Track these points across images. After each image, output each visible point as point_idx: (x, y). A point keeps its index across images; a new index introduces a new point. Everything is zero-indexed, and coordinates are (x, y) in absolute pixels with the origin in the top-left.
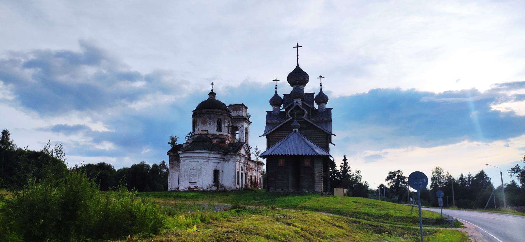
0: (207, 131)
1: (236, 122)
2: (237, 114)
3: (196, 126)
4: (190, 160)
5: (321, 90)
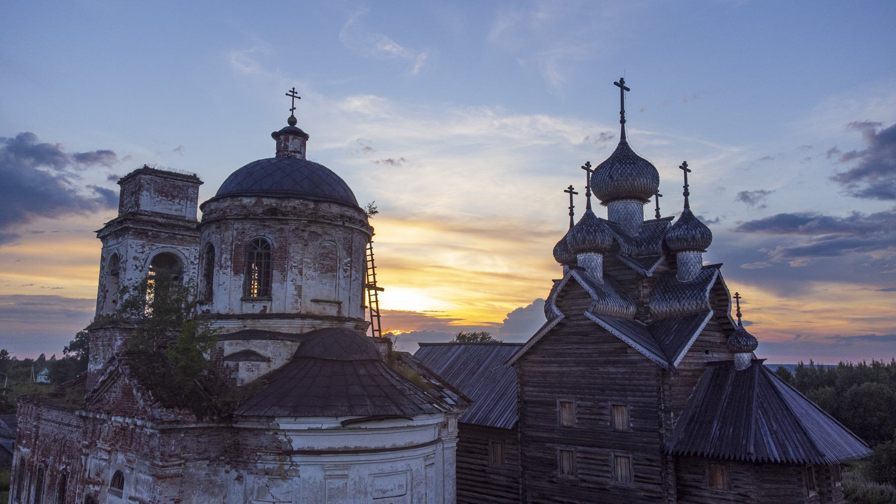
0: (339, 303)
1: (176, 239)
2: (176, 210)
3: (276, 274)
4: (374, 468)
5: (687, 205)
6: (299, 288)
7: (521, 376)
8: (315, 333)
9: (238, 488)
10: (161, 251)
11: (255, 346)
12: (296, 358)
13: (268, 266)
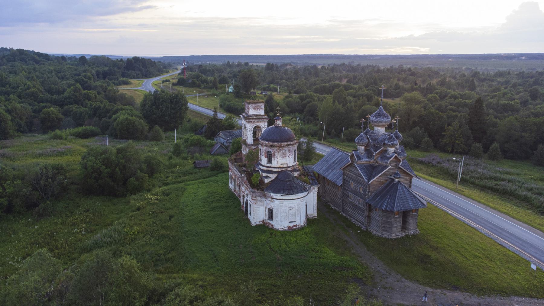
3: (273, 159)
6: (278, 162)
7: (344, 173)
8: (281, 171)
9: (265, 202)
10: (255, 125)
11: (269, 175)
12: (277, 177)
13: (271, 157)
